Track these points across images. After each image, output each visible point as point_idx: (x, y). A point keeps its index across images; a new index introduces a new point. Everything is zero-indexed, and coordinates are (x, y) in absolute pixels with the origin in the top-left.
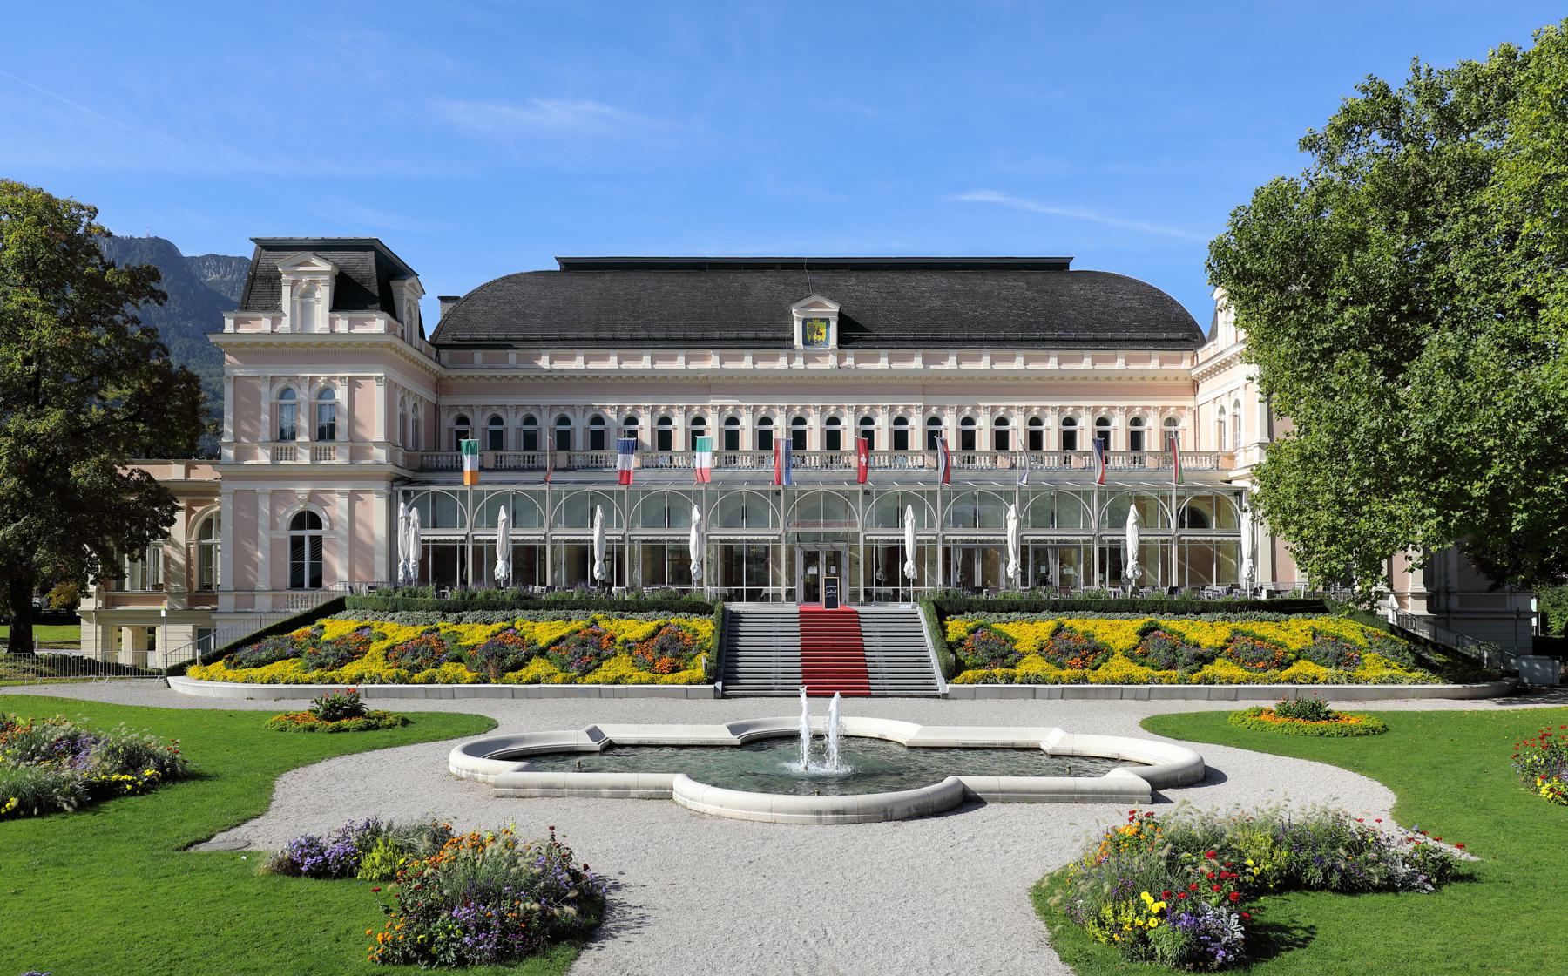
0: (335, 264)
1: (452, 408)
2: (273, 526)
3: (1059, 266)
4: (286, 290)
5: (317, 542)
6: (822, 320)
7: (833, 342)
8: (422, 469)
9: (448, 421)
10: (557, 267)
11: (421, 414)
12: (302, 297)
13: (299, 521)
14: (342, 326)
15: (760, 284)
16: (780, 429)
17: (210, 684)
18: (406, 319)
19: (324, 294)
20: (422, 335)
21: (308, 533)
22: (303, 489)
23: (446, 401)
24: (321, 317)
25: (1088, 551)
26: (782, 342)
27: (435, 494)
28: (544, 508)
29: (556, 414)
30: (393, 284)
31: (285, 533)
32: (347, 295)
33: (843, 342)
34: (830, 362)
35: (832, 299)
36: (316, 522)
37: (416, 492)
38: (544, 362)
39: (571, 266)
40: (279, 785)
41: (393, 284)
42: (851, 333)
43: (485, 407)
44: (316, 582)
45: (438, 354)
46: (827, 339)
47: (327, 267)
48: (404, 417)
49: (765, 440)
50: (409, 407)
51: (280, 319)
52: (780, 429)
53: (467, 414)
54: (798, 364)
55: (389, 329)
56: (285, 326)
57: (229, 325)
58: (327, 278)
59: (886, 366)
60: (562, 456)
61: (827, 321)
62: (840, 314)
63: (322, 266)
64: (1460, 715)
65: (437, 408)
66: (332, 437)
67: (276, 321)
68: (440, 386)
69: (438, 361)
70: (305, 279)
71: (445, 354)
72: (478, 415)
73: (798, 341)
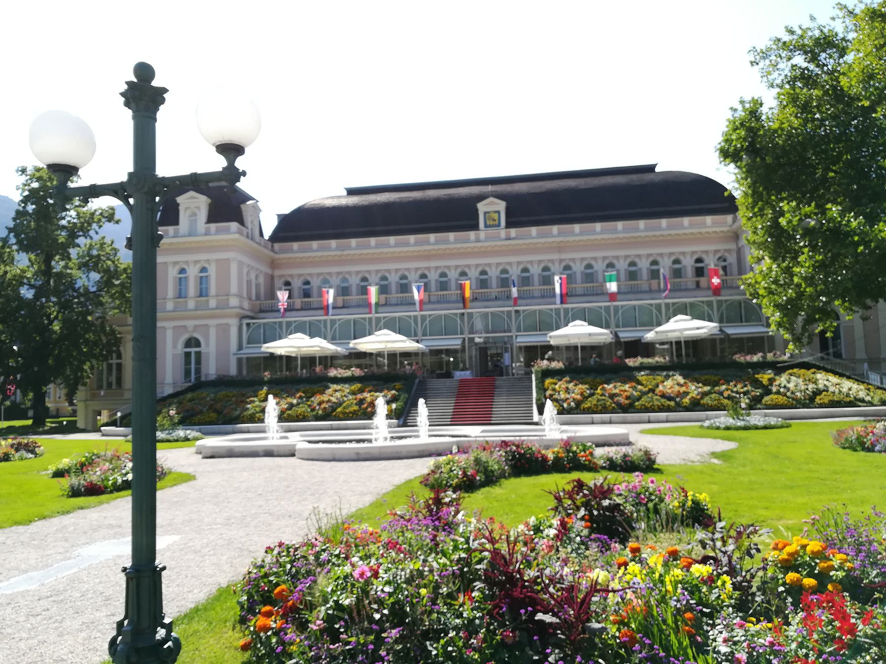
2: (175, 346)
3: (650, 169)
5: (198, 354)
6: (495, 212)
8: (261, 311)
10: (881, 300)
11: (261, 280)
18: (249, 225)
20: (261, 234)
21: (193, 350)
22: (190, 324)
23: (277, 273)
26: (475, 227)
27: (264, 324)
28: (712, 310)
29: (360, 276)
31: (180, 349)
33: (509, 225)
36: (198, 344)
37: (254, 324)
39: (351, 192)
40: (124, 178)
43: (300, 275)
45: (272, 246)
48: (249, 283)
50: (253, 276)
60: (654, 283)
65: (272, 278)
68: (273, 264)
72: (296, 280)
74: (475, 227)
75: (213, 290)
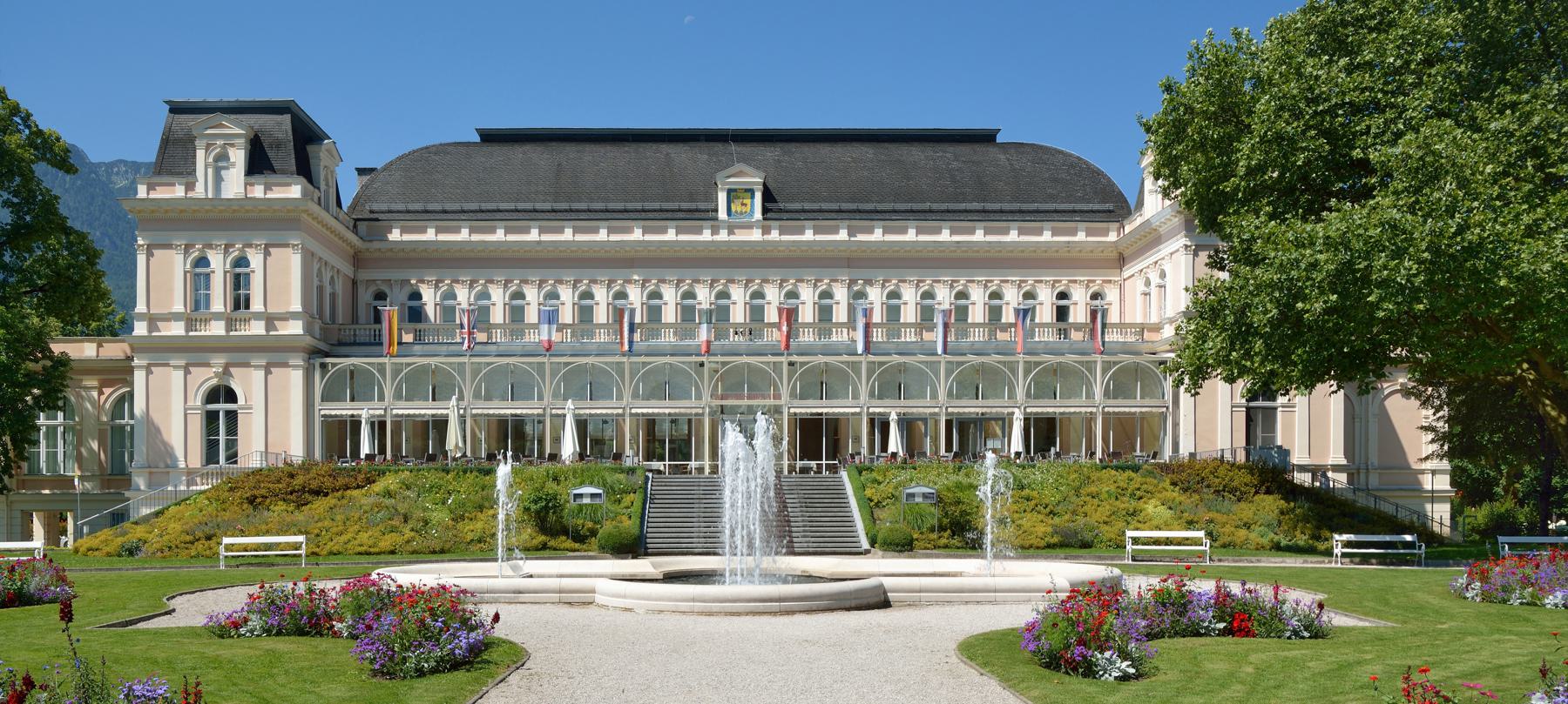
4: (200, 154)
5: (232, 417)
7: (758, 215)
9: (365, 296)
10: (478, 139)
13: (213, 396)
14: (258, 192)
18: (323, 187)
19: (238, 156)
21: (222, 407)
23: (364, 275)
24: (235, 183)
25: (937, 423)
26: (706, 215)
30: (310, 149)
34: (756, 235)
36: (231, 396)
38: (395, 235)
44: (232, 457)
46: (752, 211)
54: (723, 236)
55: (305, 193)
56: (199, 191)
61: (752, 192)
62: (765, 185)
63: (235, 128)
66: (247, 307)
67: (190, 187)
68: (358, 260)
72: (396, 289)
73: (722, 214)
74: (706, 215)
75: (257, 305)
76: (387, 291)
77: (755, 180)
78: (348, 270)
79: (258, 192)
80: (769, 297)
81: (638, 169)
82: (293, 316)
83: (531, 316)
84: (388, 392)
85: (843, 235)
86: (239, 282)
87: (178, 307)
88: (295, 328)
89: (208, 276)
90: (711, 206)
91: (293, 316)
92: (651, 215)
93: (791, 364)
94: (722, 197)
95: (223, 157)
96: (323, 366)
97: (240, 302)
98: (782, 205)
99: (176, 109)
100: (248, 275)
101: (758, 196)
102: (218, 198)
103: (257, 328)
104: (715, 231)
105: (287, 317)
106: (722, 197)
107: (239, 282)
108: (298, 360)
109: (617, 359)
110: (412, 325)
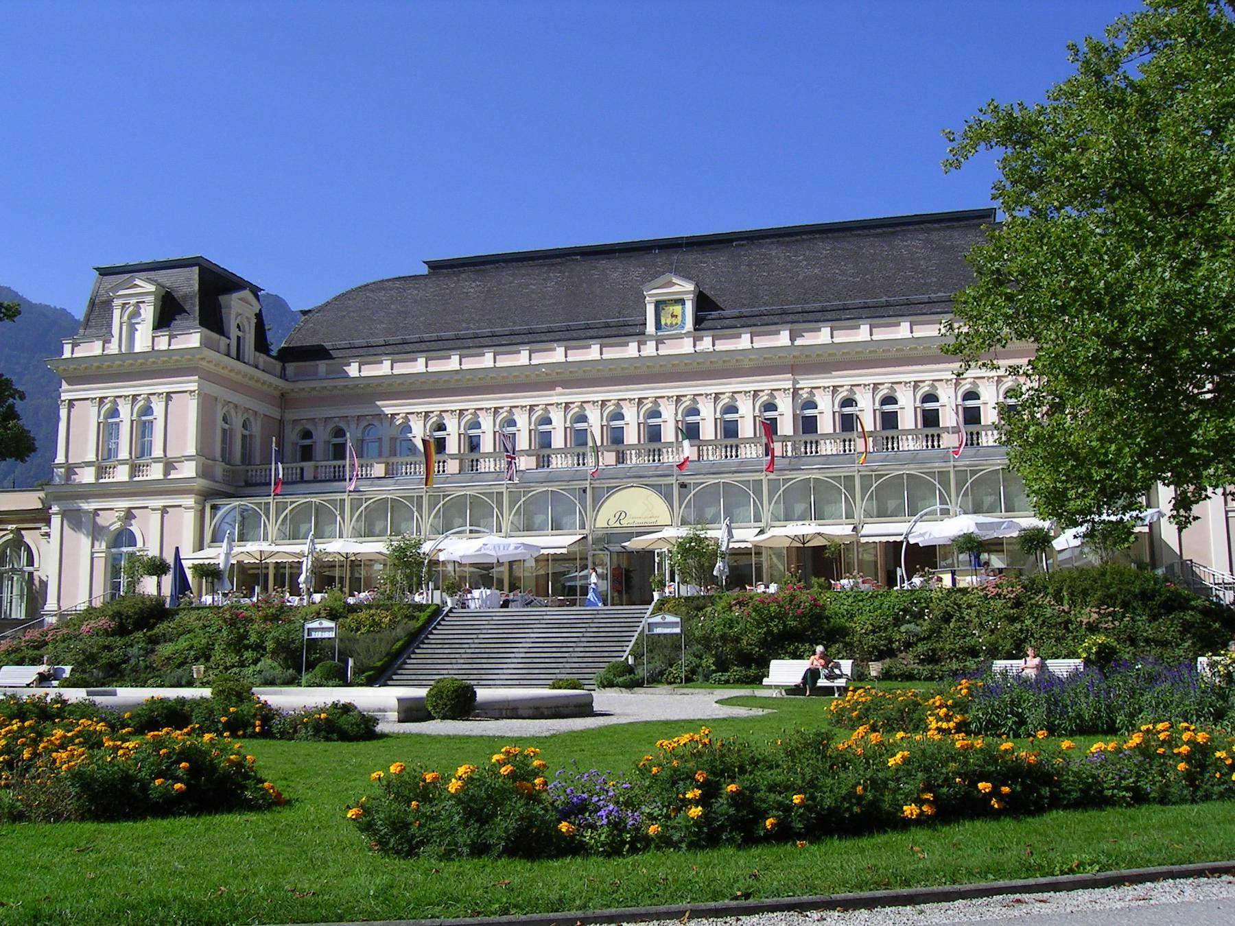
0: (159, 285)
1: (296, 422)
4: (117, 313)
7: (689, 325)
10: (425, 270)
12: (130, 318)
14: (162, 343)
15: (614, 272)
16: (867, 410)
17: (519, 872)
18: (234, 333)
19: (148, 313)
23: (291, 415)
24: (144, 339)
26: (636, 331)
30: (223, 299)
32: (168, 313)
33: (699, 322)
34: (686, 346)
35: (688, 277)
38: (353, 370)
39: (436, 267)
41: (223, 299)
42: (707, 311)
43: (327, 420)
45: (284, 369)
46: (683, 322)
47: (152, 288)
49: (848, 423)
50: (237, 422)
51: (109, 342)
52: (867, 410)
53: (310, 427)
54: (649, 349)
55: (205, 343)
56: (113, 348)
57: (67, 349)
58: (152, 298)
59: (788, 342)
61: (682, 302)
63: (145, 286)
64: (574, 735)
65: (281, 422)
67: (106, 341)
68: (284, 400)
69: (283, 376)
70: (133, 301)
71: (291, 367)
72: (320, 428)
73: (650, 328)
76: (344, 426)
77: (685, 287)
78: (275, 413)
79: (162, 343)
80: (943, 399)
81: (565, 290)
82: (189, 458)
83: (668, 434)
84: (273, 530)
85: (524, 355)
86: (143, 428)
87: (92, 457)
88: (188, 470)
89: (117, 424)
90: (639, 319)
91: (189, 458)
92: (574, 334)
93: (683, 486)
94: (650, 310)
95: (136, 314)
96: (215, 508)
97: (142, 449)
98: (726, 313)
99: (104, 272)
100: (117, 424)
101: (689, 306)
102: (131, 354)
103: (155, 472)
104: (641, 344)
105: (181, 459)
106: (650, 310)
107: (143, 428)
108: (190, 501)
109: (757, 476)
110: (614, 447)
